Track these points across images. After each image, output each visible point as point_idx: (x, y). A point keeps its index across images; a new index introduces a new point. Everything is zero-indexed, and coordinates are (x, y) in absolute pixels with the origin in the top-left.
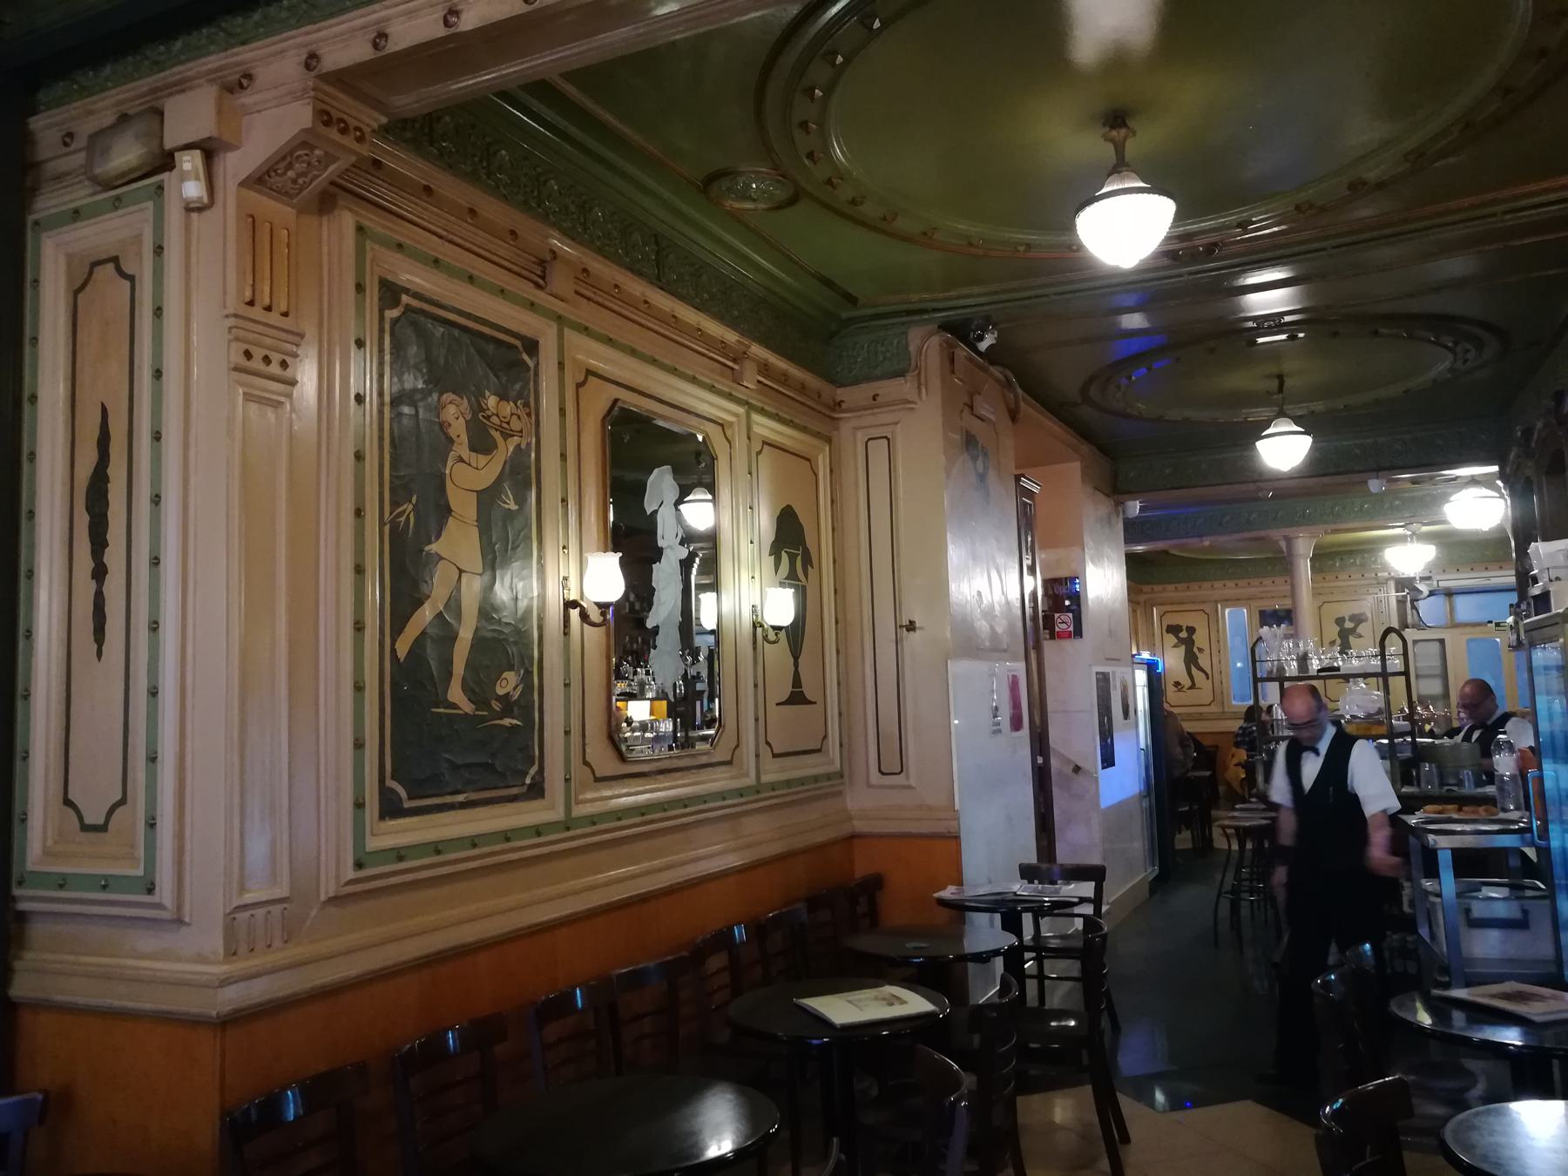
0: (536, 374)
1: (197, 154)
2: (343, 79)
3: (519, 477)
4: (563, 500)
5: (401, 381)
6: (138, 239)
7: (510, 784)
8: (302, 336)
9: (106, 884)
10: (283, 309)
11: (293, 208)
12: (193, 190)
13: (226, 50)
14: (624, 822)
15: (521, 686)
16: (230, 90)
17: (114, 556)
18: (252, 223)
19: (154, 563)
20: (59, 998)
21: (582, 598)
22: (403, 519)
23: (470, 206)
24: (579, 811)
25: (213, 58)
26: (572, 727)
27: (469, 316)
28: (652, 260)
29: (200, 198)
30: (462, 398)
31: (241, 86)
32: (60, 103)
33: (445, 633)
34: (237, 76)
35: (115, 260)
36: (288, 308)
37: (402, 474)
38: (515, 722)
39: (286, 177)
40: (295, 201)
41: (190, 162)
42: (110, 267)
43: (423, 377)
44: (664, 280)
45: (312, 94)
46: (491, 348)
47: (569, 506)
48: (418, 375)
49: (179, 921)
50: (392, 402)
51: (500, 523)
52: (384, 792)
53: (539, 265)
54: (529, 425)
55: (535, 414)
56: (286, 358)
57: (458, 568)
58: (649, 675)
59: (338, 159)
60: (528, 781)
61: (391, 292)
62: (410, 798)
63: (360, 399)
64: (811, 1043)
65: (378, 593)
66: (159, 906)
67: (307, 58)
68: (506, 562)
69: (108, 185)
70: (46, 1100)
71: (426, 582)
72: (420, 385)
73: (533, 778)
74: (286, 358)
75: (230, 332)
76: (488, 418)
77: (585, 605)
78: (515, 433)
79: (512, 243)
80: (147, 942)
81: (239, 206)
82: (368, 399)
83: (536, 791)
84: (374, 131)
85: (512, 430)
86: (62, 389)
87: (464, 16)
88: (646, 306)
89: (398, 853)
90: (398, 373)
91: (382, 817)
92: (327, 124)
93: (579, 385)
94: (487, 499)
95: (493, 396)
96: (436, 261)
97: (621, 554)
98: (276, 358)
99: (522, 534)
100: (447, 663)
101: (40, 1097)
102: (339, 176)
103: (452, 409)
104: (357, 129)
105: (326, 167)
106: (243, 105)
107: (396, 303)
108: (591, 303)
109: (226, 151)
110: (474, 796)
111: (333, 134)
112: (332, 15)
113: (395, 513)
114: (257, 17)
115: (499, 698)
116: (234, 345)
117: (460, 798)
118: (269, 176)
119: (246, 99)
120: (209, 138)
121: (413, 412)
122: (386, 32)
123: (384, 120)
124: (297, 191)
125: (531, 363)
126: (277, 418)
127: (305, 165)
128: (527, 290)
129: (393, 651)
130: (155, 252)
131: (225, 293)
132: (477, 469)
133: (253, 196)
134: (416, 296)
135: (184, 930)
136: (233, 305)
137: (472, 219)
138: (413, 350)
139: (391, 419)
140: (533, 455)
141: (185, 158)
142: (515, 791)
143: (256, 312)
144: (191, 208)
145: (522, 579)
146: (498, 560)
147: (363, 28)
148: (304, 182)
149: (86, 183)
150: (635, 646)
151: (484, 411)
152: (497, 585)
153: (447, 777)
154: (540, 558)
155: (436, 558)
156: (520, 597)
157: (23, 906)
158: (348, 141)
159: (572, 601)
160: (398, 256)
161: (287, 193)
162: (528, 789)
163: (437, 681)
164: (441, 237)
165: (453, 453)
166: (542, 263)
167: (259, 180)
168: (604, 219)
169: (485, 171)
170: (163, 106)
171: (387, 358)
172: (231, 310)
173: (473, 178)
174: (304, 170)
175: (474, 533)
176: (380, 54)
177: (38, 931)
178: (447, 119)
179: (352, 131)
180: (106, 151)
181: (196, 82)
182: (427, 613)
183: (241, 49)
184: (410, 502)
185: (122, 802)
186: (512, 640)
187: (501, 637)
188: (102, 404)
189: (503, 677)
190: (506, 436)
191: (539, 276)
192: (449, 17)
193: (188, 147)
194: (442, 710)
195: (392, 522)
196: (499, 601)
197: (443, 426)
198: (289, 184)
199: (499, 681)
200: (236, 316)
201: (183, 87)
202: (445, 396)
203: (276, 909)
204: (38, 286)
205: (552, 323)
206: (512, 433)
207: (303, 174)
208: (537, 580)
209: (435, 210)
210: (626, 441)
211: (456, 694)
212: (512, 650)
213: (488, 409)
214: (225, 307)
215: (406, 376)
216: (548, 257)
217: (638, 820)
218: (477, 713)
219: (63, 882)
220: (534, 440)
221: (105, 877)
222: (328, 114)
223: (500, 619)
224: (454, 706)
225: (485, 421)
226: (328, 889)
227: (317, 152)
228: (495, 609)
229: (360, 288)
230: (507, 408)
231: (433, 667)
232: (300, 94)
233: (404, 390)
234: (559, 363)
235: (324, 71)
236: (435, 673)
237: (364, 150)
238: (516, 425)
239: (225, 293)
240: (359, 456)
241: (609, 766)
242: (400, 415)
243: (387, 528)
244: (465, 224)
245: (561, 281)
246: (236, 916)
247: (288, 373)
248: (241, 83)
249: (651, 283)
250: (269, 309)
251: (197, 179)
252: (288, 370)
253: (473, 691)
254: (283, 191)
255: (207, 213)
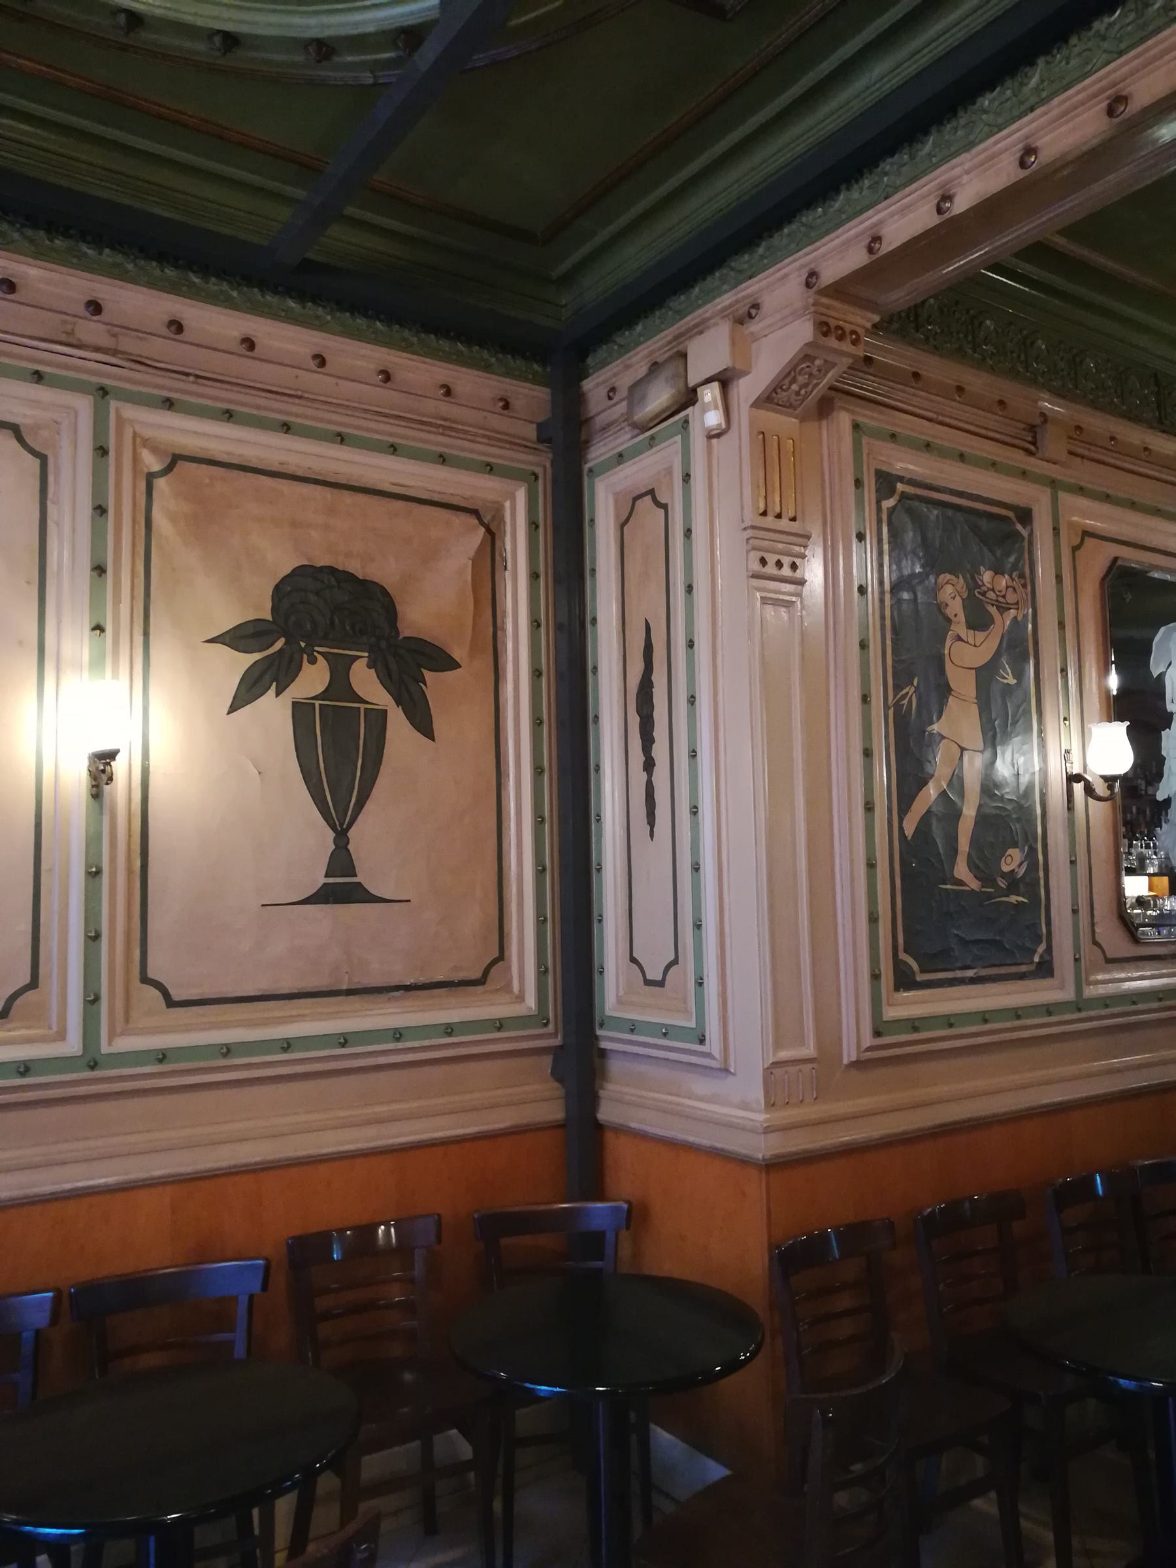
0: (1031, 543)
1: (716, 385)
2: (840, 290)
3: (1017, 650)
4: (1062, 670)
5: (900, 569)
6: (669, 472)
7: (1019, 962)
8: (808, 537)
9: (667, 1032)
10: (792, 514)
11: (796, 418)
12: (713, 418)
13: (736, 287)
14: (1140, 1007)
15: (1025, 864)
16: (740, 321)
17: (660, 751)
18: (762, 437)
19: (692, 756)
20: (633, 1125)
21: (1085, 771)
22: (905, 702)
23: (914, 370)
24: (1090, 991)
25: (726, 296)
26: (1080, 904)
27: (960, 494)
28: (1153, 403)
29: (720, 425)
30: (958, 578)
31: (750, 316)
32: (604, 364)
33: (950, 811)
34: (746, 308)
35: (651, 492)
36: (796, 512)
37: (903, 658)
38: (1021, 899)
39: (790, 391)
40: (797, 412)
41: (710, 394)
42: (648, 498)
43: (920, 561)
44: (1167, 422)
45: (812, 309)
46: (984, 524)
47: (1069, 675)
48: (916, 560)
49: (726, 1070)
50: (892, 590)
51: (999, 700)
52: (899, 967)
53: (1030, 431)
54: (1025, 597)
55: (1028, 581)
56: (796, 560)
57: (959, 746)
58: (1150, 848)
59: (835, 364)
60: (1036, 959)
61: (886, 482)
62: (922, 971)
63: (862, 590)
64: (1117, 1382)
65: (885, 775)
66: (708, 1055)
67: (808, 277)
68: (1007, 736)
69: (643, 428)
70: (630, 1211)
71: (930, 762)
72: (918, 570)
73: (1041, 957)
74: (796, 560)
75: (747, 543)
76: (984, 594)
77: (1090, 779)
78: (1011, 606)
79: (1000, 413)
80: (701, 1085)
81: (752, 424)
82: (870, 589)
83: (1045, 969)
84: (867, 330)
85: (1008, 603)
86: (614, 609)
87: (957, 200)
88: (1146, 453)
89: (1016, 1012)
90: (896, 561)
91: (897, 988)
92: (825, 334)
93: (1075, 549)
94: (985, 675)
95: (987, 572)
96: (928, 445)
97: (1128, 723)
98: (786, 561)
99: (1021, 709)
100: (952, 841)
101: (625, 1206)
102: (837, 381)
103: (949, 589)
104: (853, 332)
105: (825, 375)
106: (752, 333)
107: (892, 492)
108: (1085, 461)
109: (739, 378)
110: (984, 972)
111: (832, 342)
112: (827, 233)
113: (898, 697)
114: (761, 250)
115: (1004, 875)
116: (752, 554)
117: (970, 973)
118: (776, 393)
119: (754, 327)
120: (726, 369)
121: (912, 597)
122: (880, 235)
123: (876, 318)
124: (799, 402)
125: (1025, 533)
126: (789, 617)
127: (807, 376)
128: (1017, 458)
129: (901, 829)
130: (684, 480)
131: (742, 508)
132: (975, 646)
133: (762, 414)
134: (912, 482)
135: (730, 1078)
136: (751, 517)
137: (960, 397)
138: (909, 536)
139: (892, 606)
140: (1030, 626)
141: (705, 392)
142: (1024, 968)
143: (769, 521)
144: (714, 435)
145: (1023, 754)
146: (999, 735)
147: (857, 236)
148: (806, 392)
149: (627, 429)
150: (1129, 816)
151: (979, 587)
152: (999, 763)
153: (957, 953)
154: (1040, 731)
155: (938, 739)
156: (1021, 772)
157: (604, 1045)
158: (846, 346)
159: (1076, 775)
160: (892, 445)
161: (791, 406)
162: (1037, 967)
163: (943, 858)
164: (929, 420)
165: (950, 633)
166: (1032, 428)
167: (768, 400)
168: (1096, 369)
169: (970, 346)
170: (686, 347)
171: (886, 547)
172: (748, 523)
173: (959, 355)
174: (806, 381)
175: (975, 709)
176: (874, 257)
177: (615, 1066)
178: (932, 301)
179: (848, 336)
180: (643, 398)
181: (712, 321)
182: (931, 791)
183: (750, 282)
184: (912, 684)
185: (675, 962)
186: (1014, 816)
187: (1004, 814)
188: (646, 620)
189: (1007, 853)
190: (1003, 609)
191: (1030, 442)
192: (942, 204)
193: (708, 381)
194: (949, 887)
195: (897, 705)
196: (1001, 778)
197: (940, 608)
198: (793, 397)
199: (1003, 859)
200: (753, 527)
201: (700, 328)
202: (942, 576)
203: (808, 1067)
204: (594, 524)
205: (1045, 488)
206: (1008, 606)
207: (806, 385)
208: (1038, 754)
209: (922, 393)
210: (1128, 600)
211: (962, 870)
212: (1016, 827)
213: (984, 585)
214: (743, 522)
215: (904, 563)
216: (1038, 421)
217: (1155, 1005)
218: (983, 890)
219: (633, 1027)
220: (1030, 610)
221: (665, 1026)
222: (827, 324)
223: (1003, 795)
224: (960, 883)
225: (981, 597)
226: (849, 1054)
227: (817, 362)
228: (997, 786)
229: (858, 483)
230: (1003, 582)
231: (940, 846)
232: (802, 312)
233: (902, 576)
234: (1054, 529)
235: (823, 286)
236: (941, 851)
237: (860, 352)
238: (1011, 598)
239: (742, 508)
240: (863, 645)
241: (1125, 948)
242: (900, 601)
243: (891, 712)
244: (954, 404)
245: (1054, 443)
246: (773, 1071)
247: (798, 574)
248: (750, 312)
249: (1151, 427)
250: (779, 516)
251: (716, 408)
252: (798, 571)
253: (977, 867)
254: (788, 404)
255: (724, 438)
